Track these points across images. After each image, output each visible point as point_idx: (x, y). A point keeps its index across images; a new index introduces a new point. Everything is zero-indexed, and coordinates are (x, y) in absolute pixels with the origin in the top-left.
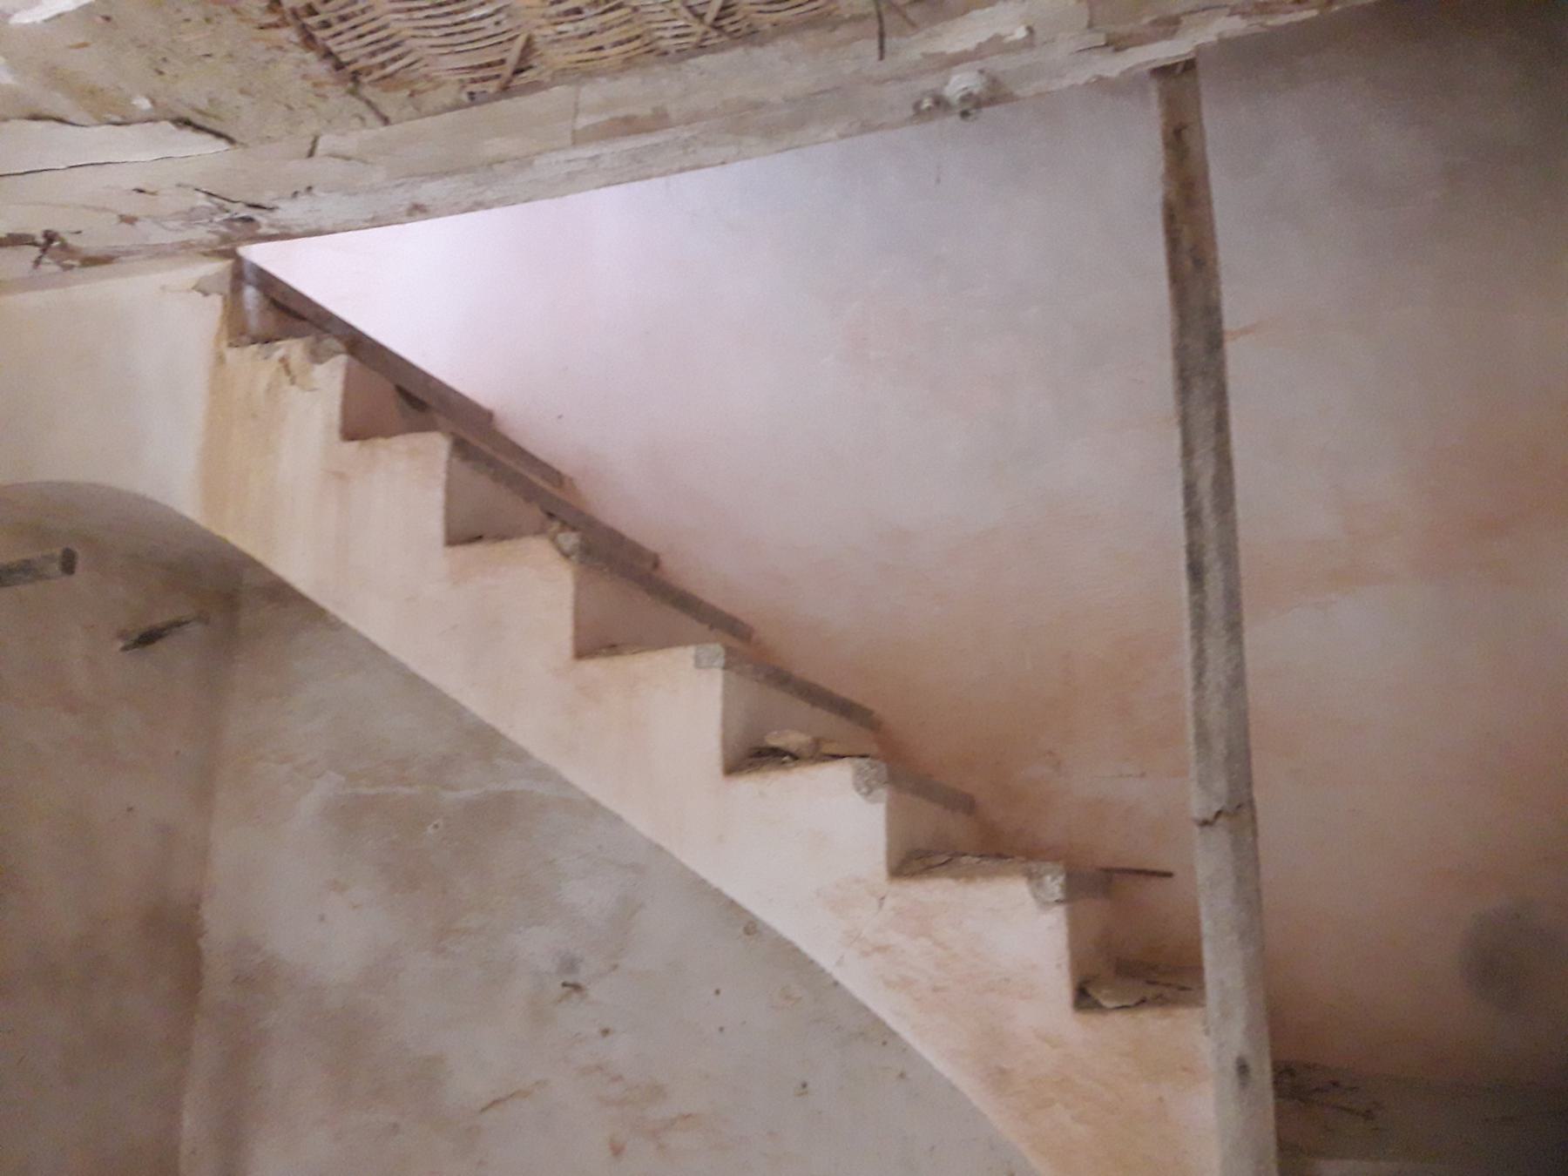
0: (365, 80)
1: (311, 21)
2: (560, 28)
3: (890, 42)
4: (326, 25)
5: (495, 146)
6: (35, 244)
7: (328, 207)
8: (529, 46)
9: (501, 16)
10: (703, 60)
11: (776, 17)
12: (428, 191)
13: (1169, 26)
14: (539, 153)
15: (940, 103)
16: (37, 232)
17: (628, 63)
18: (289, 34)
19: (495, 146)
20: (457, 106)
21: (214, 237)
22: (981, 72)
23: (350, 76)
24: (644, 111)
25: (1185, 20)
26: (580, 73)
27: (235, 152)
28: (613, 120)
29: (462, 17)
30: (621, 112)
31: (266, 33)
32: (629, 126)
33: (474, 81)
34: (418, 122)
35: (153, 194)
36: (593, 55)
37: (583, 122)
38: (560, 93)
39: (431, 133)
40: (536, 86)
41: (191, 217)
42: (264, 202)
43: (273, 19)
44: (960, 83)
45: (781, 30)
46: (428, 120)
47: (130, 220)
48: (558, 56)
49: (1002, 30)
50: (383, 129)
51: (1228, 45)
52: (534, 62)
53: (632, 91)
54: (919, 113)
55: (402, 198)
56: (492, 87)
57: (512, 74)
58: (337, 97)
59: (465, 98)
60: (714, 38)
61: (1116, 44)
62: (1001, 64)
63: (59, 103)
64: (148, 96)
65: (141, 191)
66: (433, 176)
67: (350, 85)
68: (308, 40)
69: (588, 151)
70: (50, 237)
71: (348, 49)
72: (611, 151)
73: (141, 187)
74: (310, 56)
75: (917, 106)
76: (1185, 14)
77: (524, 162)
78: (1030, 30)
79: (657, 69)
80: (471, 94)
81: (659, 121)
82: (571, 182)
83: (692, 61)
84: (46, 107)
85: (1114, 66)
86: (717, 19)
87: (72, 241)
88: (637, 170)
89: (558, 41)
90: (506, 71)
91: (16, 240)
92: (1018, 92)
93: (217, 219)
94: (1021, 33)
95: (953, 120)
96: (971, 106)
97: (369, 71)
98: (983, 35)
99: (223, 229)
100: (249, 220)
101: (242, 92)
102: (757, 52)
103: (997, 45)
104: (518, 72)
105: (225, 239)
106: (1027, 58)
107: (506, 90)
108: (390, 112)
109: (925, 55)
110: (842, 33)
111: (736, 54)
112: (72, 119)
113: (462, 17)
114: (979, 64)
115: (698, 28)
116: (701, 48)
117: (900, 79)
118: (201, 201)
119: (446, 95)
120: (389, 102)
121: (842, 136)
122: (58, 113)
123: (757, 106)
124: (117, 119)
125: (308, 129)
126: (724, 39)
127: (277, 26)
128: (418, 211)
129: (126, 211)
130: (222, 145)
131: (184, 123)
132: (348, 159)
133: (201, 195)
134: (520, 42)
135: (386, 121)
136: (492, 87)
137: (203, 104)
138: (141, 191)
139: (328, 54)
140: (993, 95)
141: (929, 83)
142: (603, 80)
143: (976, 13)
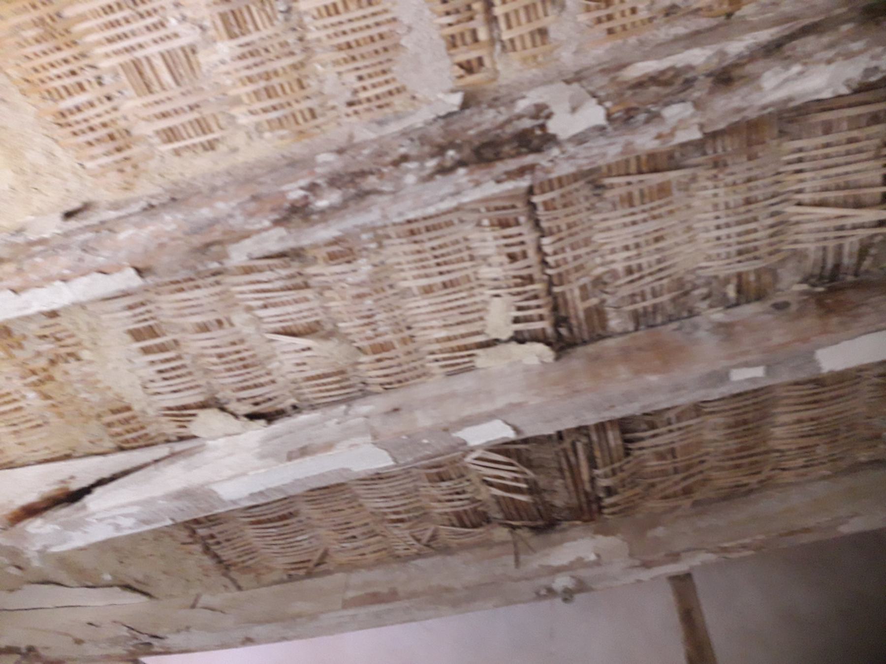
0: (233, 568)
1: (211, 541)
2: (344, 545)
3: (522, 557)
4: (218, 543)
5: (300, 606)
6: (20, 653)
7: (196, 637)
8: (325, 554)
9: (312, 540)
10: (419, 562)
11: (457, 541)
12: (257, 631)
13: (675, 557)
14: (322, 613)
15: (551, 592)
16: (23, 645)
17: (379, 563)
18: (197, 548)
19: (300, 606)
20: (281, 582)
21: (125, 652)
22: (573, 577)
23: (224, 566)
24: (384, 590)
25: (683, 555)
26: (350, 567)
27: (154, 602)
28: (367, 594)
29: (292, 540)
30: (371, 590)
31: (185, 546)
32: (375, 598)
33: (293, 569)
34: (257, 590)
35: (97, 626)
36: (359, 557)
37: (350, 594)
38: (339, 577)
39: (263, 598)
40: (328, 572)
41: (114, 641)
42: (159, 634)
43: (190, 540)
44: (562, 582)
45: (463, 547)
46: (265, 589)
47: (79, 642)
48: (342, 558)
49: (582, 555)
50: (237, 593)
51: (705, 566)
52: (327, 560)
53: (378, 578)
54: (539, 597)
55: (240, 634)
56: (302, 572)
57: (314, 567)
58: (217, 578)
59: (285, 577)
60: (427, 550)
61: (647, 565)
62: (583, 573)
63: (62, 576)
64: (111, 574)
65: (91, 624)
66: (260, 623)
67: (224, 571)
68: (207, 550)
69: (352, 611)
70: (31, 649)
71: (226, 554)
72: (363, 612)
73: (90, 620)
74: (205, 558)
75: (537, 593)
76: (684, 551)
77: (313, 617)
78: (598, 556)
79: (395, 566)
80: (290, 575)
81: (393, 596)
82: (339, 628)
83: (414, 562)
84: (52, 577)
85: (645, 575)
86: (429, 541)
87: (43, 653)
88: (378, 622)
89: (340, 551)
90: (311, 565)
91: (10, 650)
92: (593, 586)
93: (131, 643)
94: (593, 557)
95: (558, 601)
96: (568, 595)
97: (235, 564)
98: (572, 558)
99: (131, 648)
100: (149, 644)
101: (165, 573)
102: (449, 558)
103: (580, 563)
104: (318, 565)
105: (132, 653)
106: (597, 571)
107: (310, 575)
108: (242, 583)
109: (541, 566)
110: (495, 550)
111: (437, 559)
112: (67, 583)
113: (292, 540)
114: (571, 573)
115: (418, 545)
116: (419, 555)
117: (527, 579)
118: (124, 632)
119: (275, 576)
120: (243, 580)
121: (496, 606)
122: (58, 580)
123: (448, 590)
124: (90, 584)
125: (193, 592)
126: (431, 551)
127: (191, 543)
128: (248, 641)
129: (80, 636)
130: (144, 599)
131: (127, 587)
132: (213, 609)
133: (125, 628)
134: (320, 552)
135: (239, 588)
136: (302, 572)
137: (140, 577)
138: (91, 624)
139: (216, 556)
140: (582, 587)
141: (544, 581)
142: (363, 570)
143: (567, 544)
